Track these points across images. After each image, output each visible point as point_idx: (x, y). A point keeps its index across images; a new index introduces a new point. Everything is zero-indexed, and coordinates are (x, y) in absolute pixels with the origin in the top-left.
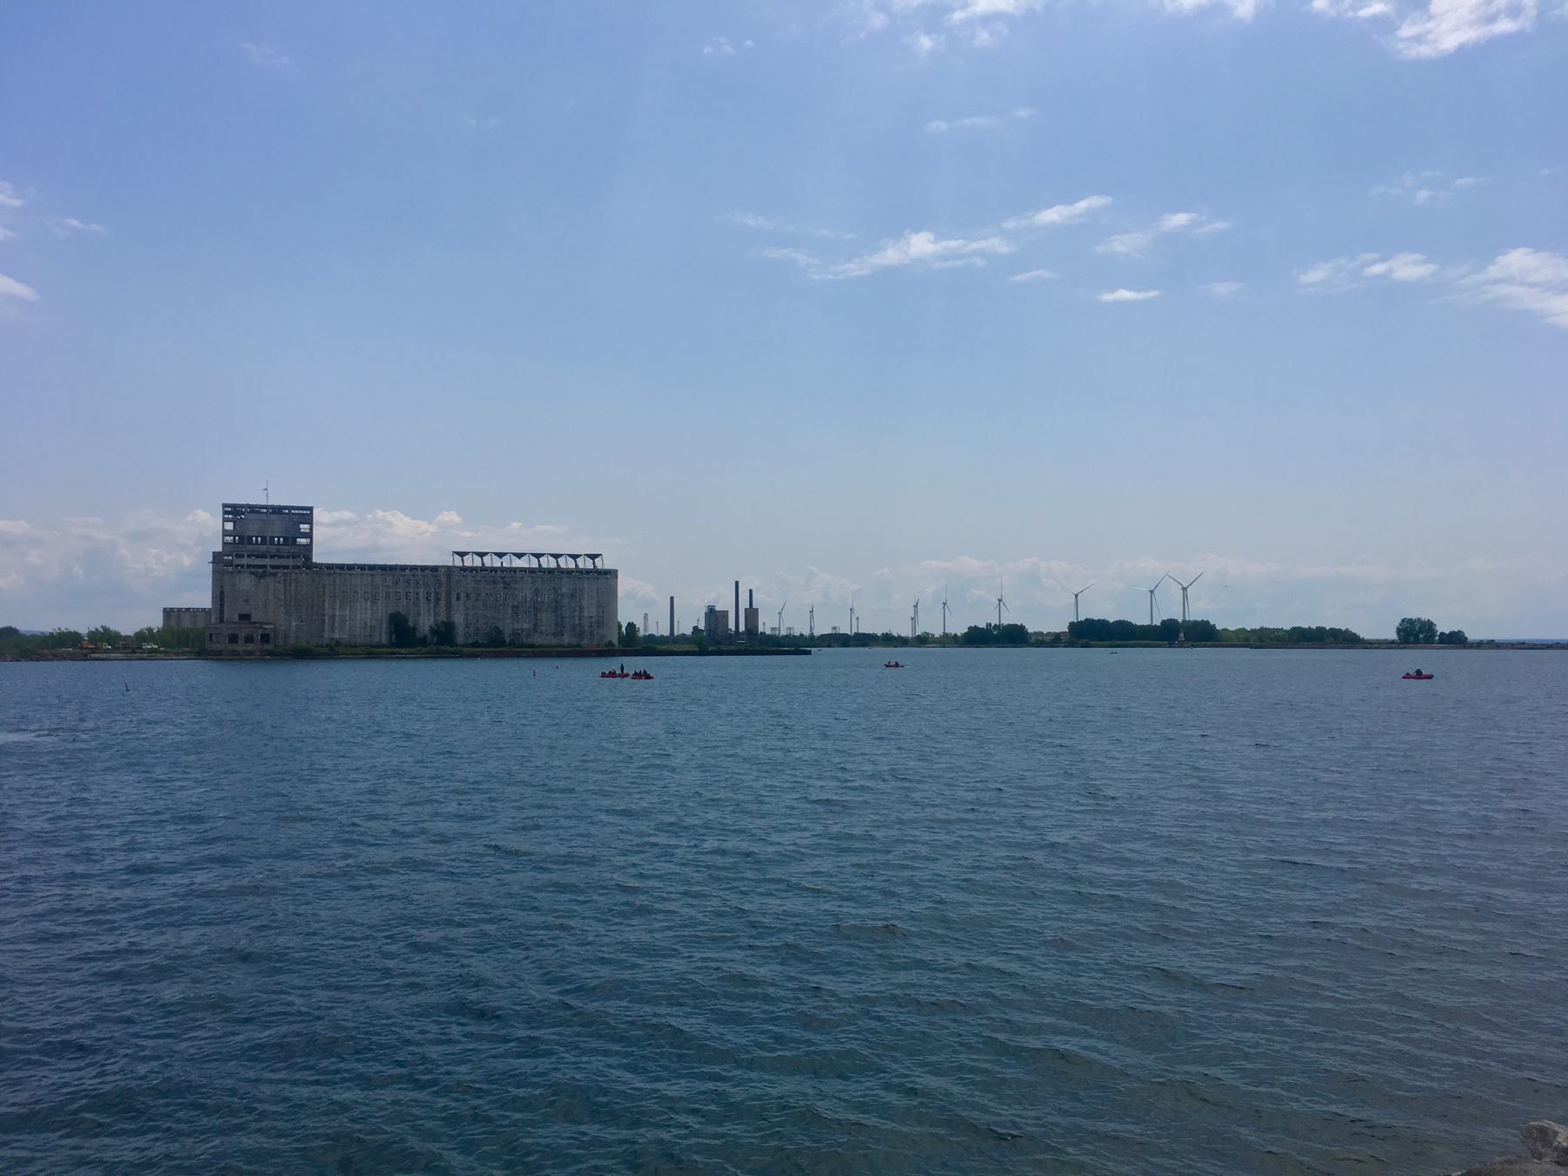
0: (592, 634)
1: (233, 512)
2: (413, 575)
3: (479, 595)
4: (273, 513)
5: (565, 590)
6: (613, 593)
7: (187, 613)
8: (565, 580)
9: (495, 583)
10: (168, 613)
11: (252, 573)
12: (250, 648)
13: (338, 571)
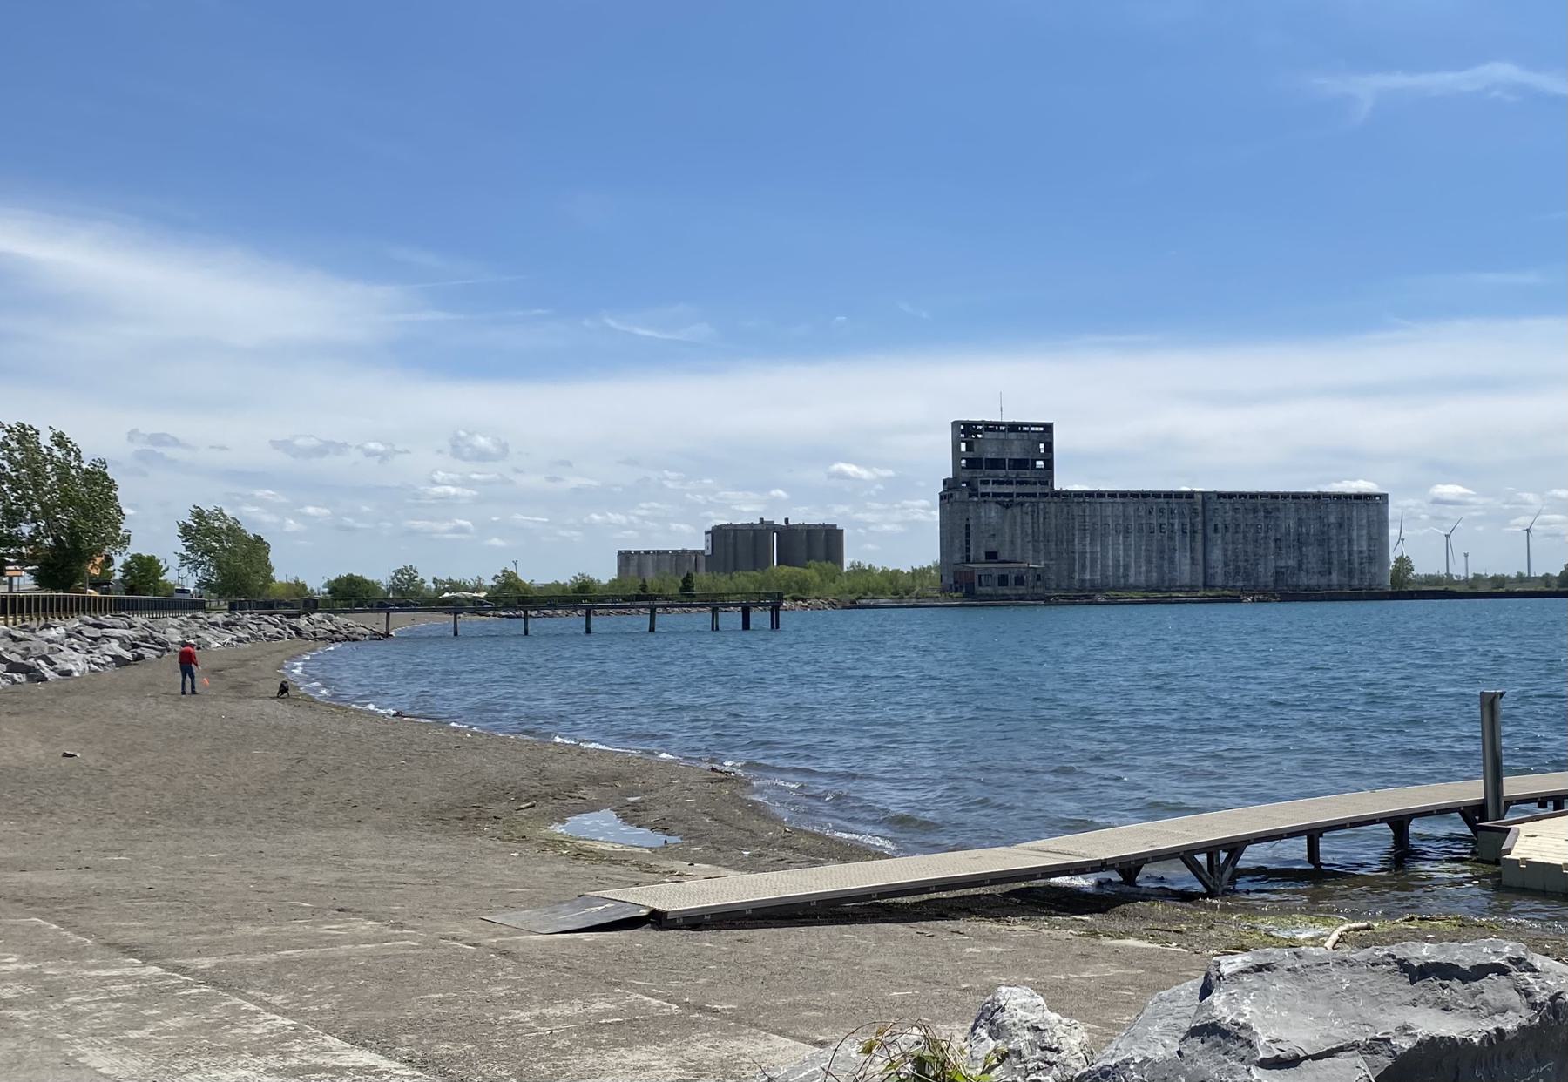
0: (1362, 572)
1: (966, 430)
2: (1168, 503)
3: (1238, 525)
4: (1010, 431)
5: (1332, 519)
6: (1382, 523)
7: (636, 557)
8: (1332, 507)
9: (1255, 511)
10: (625, 557)
11: (997, 503)
12: (1020, 592)
13: (1087, 499)
